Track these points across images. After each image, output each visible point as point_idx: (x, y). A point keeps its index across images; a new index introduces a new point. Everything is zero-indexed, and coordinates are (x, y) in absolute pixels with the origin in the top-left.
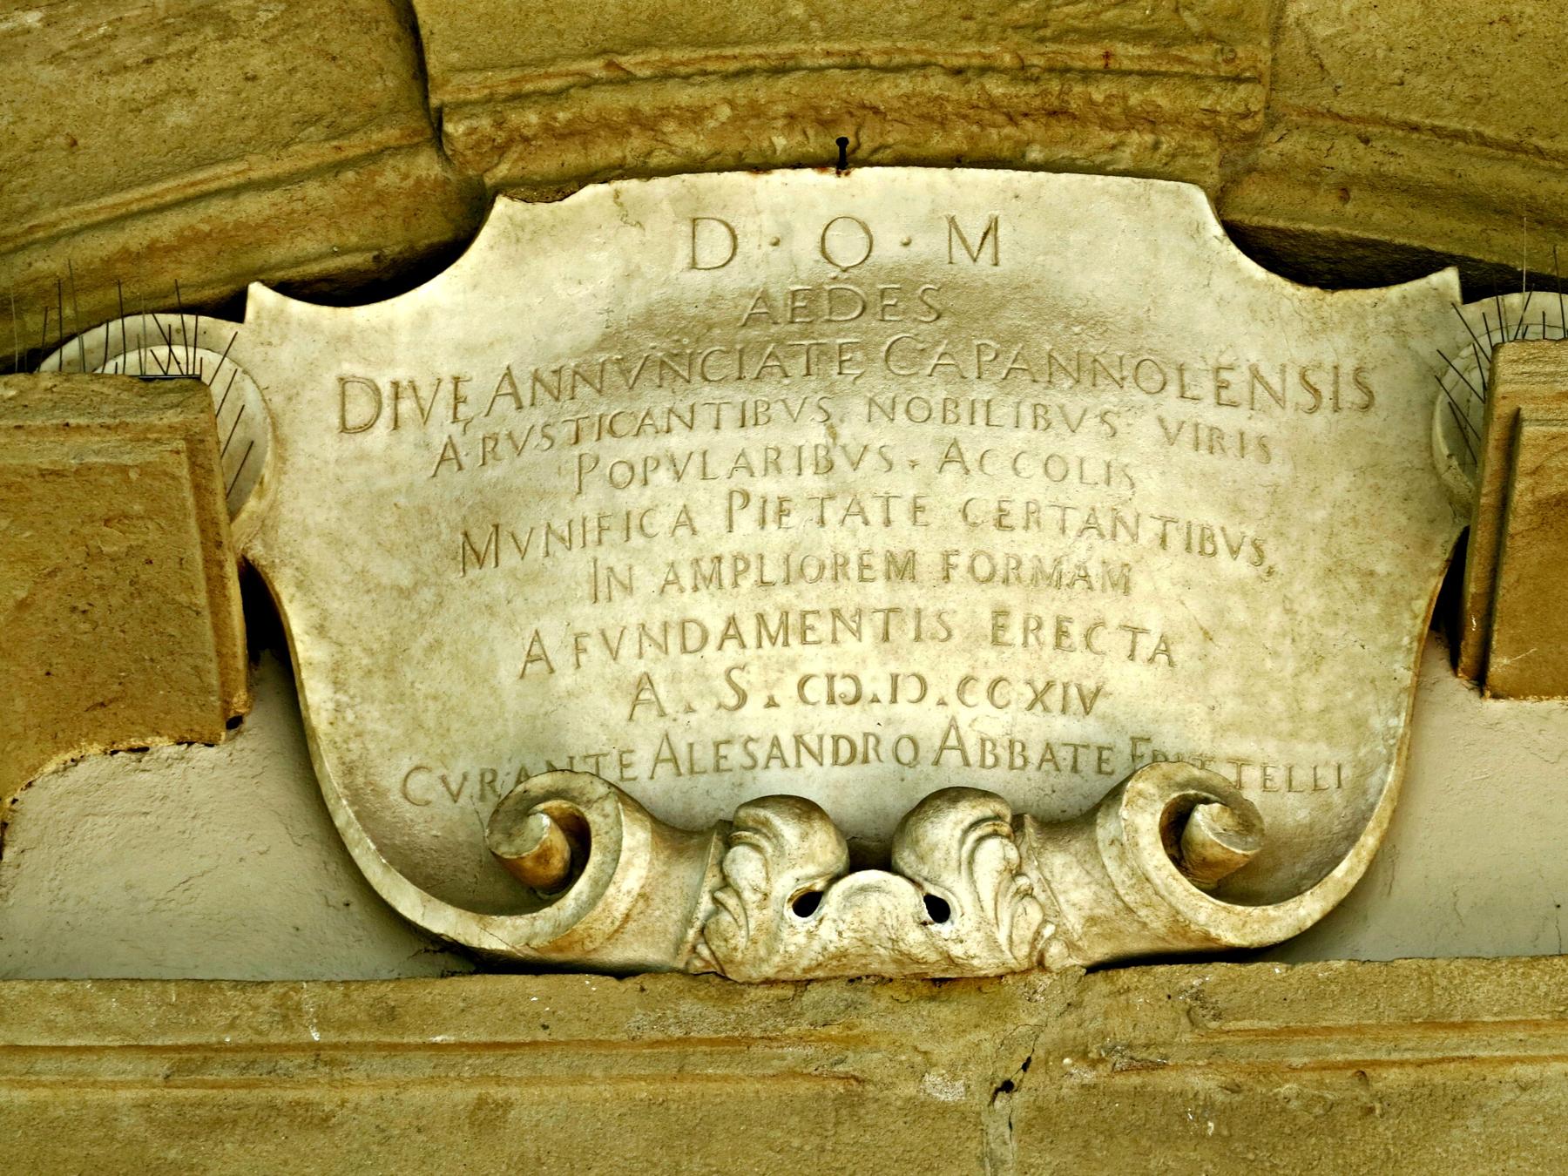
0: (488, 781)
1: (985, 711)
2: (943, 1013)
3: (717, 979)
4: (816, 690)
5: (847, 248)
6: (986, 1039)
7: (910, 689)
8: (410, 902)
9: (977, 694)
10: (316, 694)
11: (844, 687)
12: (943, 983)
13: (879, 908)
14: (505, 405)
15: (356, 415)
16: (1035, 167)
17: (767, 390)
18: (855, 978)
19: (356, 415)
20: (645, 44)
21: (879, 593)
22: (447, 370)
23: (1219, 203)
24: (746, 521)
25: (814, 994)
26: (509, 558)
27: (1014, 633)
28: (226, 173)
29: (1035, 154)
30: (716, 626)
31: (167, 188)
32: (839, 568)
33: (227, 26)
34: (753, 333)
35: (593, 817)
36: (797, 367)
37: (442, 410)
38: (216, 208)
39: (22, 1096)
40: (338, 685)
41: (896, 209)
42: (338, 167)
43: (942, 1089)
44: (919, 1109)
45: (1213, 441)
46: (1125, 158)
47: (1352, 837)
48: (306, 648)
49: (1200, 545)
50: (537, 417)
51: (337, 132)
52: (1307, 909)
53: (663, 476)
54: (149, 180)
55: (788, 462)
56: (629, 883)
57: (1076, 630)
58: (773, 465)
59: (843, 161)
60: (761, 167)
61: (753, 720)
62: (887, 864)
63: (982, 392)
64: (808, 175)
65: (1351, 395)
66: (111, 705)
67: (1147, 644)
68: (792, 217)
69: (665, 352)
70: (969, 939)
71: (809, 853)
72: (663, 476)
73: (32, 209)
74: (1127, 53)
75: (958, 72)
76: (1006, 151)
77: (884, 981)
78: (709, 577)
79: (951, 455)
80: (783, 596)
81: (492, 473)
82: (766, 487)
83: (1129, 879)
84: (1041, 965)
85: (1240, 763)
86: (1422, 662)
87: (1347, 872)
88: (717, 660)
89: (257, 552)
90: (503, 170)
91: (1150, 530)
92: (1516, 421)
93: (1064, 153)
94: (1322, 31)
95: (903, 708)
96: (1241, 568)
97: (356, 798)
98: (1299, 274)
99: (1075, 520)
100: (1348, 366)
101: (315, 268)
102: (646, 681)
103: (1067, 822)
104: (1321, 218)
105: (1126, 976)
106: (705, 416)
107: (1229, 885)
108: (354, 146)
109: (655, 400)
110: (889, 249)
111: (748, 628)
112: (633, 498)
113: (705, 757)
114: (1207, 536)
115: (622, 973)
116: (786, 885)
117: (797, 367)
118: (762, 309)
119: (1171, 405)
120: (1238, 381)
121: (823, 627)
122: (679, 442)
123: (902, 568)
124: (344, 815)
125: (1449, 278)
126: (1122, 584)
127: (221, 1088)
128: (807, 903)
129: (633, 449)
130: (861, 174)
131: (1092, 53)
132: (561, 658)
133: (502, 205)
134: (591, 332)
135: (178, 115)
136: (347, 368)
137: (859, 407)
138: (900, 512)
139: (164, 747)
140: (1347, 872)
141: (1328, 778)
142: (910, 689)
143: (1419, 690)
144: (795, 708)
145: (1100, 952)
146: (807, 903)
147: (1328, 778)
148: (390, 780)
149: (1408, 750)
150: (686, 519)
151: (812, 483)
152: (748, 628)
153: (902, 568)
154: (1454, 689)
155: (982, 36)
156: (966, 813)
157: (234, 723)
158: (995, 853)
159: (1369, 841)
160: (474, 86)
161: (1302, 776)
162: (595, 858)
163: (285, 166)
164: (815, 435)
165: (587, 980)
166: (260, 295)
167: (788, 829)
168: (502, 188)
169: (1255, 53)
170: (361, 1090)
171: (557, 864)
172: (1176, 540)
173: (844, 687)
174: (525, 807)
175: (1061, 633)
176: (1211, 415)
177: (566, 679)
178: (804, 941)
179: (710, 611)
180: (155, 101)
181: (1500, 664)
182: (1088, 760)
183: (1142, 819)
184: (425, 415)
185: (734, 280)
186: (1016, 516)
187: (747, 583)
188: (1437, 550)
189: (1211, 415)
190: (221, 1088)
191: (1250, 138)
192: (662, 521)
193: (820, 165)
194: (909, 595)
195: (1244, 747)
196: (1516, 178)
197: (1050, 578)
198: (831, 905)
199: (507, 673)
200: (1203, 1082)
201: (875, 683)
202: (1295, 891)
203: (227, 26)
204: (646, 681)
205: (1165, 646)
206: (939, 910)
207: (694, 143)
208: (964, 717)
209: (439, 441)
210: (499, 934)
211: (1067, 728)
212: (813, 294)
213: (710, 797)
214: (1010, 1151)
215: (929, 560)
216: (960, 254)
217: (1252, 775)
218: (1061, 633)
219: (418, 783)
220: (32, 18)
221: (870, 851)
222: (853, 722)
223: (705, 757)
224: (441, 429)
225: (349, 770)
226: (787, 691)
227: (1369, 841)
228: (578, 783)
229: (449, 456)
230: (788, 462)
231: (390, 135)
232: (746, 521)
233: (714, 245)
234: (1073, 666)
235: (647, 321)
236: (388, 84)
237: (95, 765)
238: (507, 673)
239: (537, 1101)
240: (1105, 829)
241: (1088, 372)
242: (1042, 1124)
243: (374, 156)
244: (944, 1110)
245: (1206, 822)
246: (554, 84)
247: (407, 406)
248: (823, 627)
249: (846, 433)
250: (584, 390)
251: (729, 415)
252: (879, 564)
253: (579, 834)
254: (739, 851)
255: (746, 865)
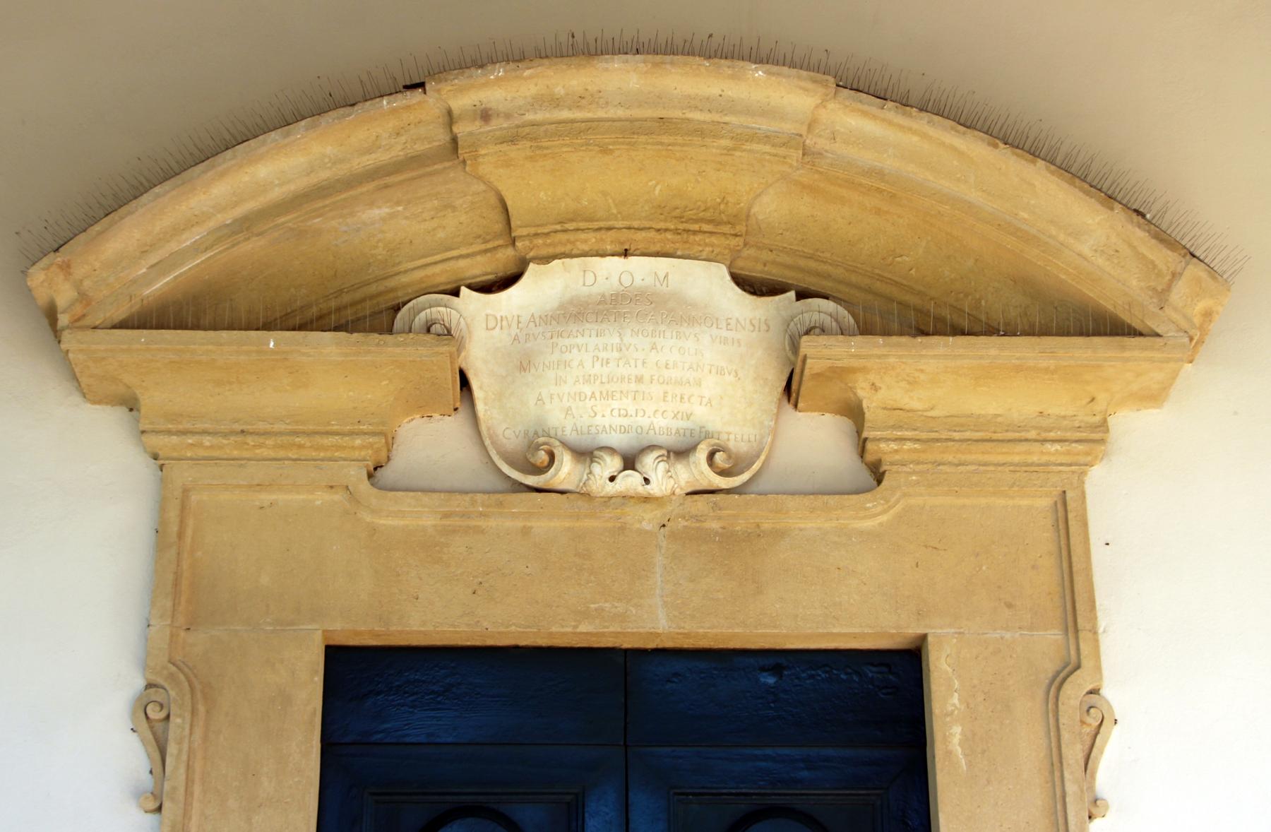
0: (526, 433)
1: (661, 422)
2: (648, 506)
3: (587, 496)
4: (616, 413)
5: (627, 282)
6: (658, 513)
7: (641, 413)
8: (506, 469)
9: (659, 415)
10: (480, 407)
11: (623, 412)
12: (647, 499)
13: (630, 482)
14: (532, 325)
15: (491, 325)
16: (679, 257)
17: (604, 326)
18: (625, 498)
19: (491, 325)
20: (572, 220)
21: (633, 386)
22: (515, 314)
23: (729, 268)
24: (598, 365)
25: (613, 500)
26: (533, 371)
27: (669, 398)
28: (455, 253)
29: (679, 253)
30: (589, 394)
31: (438, 258)
32: (623, 379)
33: (454, 209)
34: (600, 307)
35: (555, 451)
36: (612, 318)
37: (514, 325)
38: (451, 264)
39: (402, 523)
40: (486, 404)
41: (641, 270)
42: (486, 251)
43: (646, 526)
44: (641, 532)
45: (725, 341)
46: (704, 255)
47: (758, 456)
48: (478, 393)
49: (720, 372)
50: (540, 329)
51: (486, 242)
52: (745, 477)
53: (575, 351)
54: (433, 255)
55: (609, 348)
56: (565, 472)
57: (686, 398)
58: (605, 349)
59: (626, 254)
60: (603, 255)
61: (599, 420)
62: (634, 469)
63: (663, 328)
64: (616, 258)
65: (764, 327)
66: (422, 405)
67: (705, 401)
68: (611, 273)
69: (577, 312)
70: (655, 489)
71: (613, 464)
72: (575, 351)
73: (399, 263)
74: (706, 227)
75: (659, 230)
76: (671, 251)
77: (632, 497)
78: (588, 380)
79: (654, 348)
80: (607, 386)
81: (528, 345)
82: (603, 355)
83: (697, 472)
84: (674, 494)
85: (729, 433)
86: (779, 407)
87: (756, 467)
88: (589, 403)
89: (464, 366)
90: (531, 254)
91: (707, 368)
92: (805, 358)
93: (687, 252)
94: (760, 217)
95: (639, 418)
96: (732, 378)
97: (491, 437)
98: (754, 293)
99: (687, 366)
100: (763, 319)
101: (479, 279)
102: (569, 408)
103: (680, 453)
104: (756, 271)
105: (696, 497)
106: (587, 332)
107: (723, 473)
108: (489, 245)
109: (573, 327)
110: (638, 282)
111: (598, 395)
112: (567, 356)
113: (585, 430)
114: (722, 369)
115: (562, 492)
116: (607, 474)
117: (612, 318)
118: (603, 300)
119: (714, 331)
120: (733, 322)
121: (618, 395)
122: (580, 340)
123: (639, 380)
124: (487, 442)
125: (792, 294)
126: (699, 384)
127: (455, 522)
128: (612, 479)
129: (567, 342)
130: (630, 258)
131: (696, 227)
132: (547, 400)
133: (532, 266)
134: (556, 305)
135: (441, 234)
136: (489, 312)
137: (629, 331)
138: (639, 363)
139: (437, 416)
140: (756, 467)
141: (752, 438)
142: (641, 413)
143: (777, 417)
144: (612, 420)
145: (689, 490)
146: (612, 479)
147: (752, 438)
148: (500, 432)
149: (775, 433)
150: (581, 364)
151: (616, 354)
152: (598, 395)
153: (639, 380)
154: (788, 408)
155: (665, 221)
156: (655, 454)
157: (456, 409)
158: (662, 466)
159: (763, 457)
160: (524, 232)
161: (746, 437)
162: (556, 463)
163: (470, 251)
164: (616, 340)
165: (553, 495)
166: (464, 290)
167: (608, 458)
168: (533, 259)
169: (740, 228)
170: (493, 523)
171: (546, 463)
172: (714, 371)
173: (623, 412)
174: (537, 447)
175: (682, 398)
176: (725, 333)
177: (548, 406)
178: (611, 488)
179: (587, 390)
180: (434, 229)
181: (800, 405)
182: (688, 433)
183: (701, 455)
184: (510, 326)
185: (596, 290)
186: (671, 365)
187: (598, 382)
188: (804, 206)
189: (725, 333)
190: (455, 522)
191: (739, 251)
192: (575, 364)
193: (619, 255)
194: (642, 387)
195: (730, 429)
196: (812, 264)
197: (679, 383)
198: (618, 480)
199: (532, 402)
200: (715, 525)
201: (631, 411)
202: (741, 472)
203: (454, 209)
204: (569, 408)
205: (710, 401)
206: (647, 481)
207: (586, 248)
208: (655, 421)
209: (513, 334)
210: (531, 480)
211: (683, 424)
212: (617, 295)
213: (585, 442)
214: (664, 544)
215: (647, 378)
216: (658, 284)
217: (732, 437)
218: (682, 398)
219: (507, 432)
220: (400, 208)
221: (630, 463)
222: (625, 422)
223: (585, 430)
224: (514, 331)
225: (489, 429)
226: (608, 413)
227: (763, 457)
228: (552, 440)
229: (516, 338)
230: (609, 348)
231: (500, 242)
232: (598, 365)
233: (590, 279)
234: (685, 407)
235: (571, 302)
236: (499, 227)
237: (418, 421)
238: (532, 402)
239: (540, 526)
240: (692, 459)
241: (692, 321)
242: (673, 536)
243: (495, 248)
244: (647, 532)
245: (719, 457)
246: (546, 231)
247: (505, 323)
248: (618, 395)
249: (625, 339)
250: (554, 322)
251: (594, 333)
252: (633, 378)
253: (552, 456)
254: (595, 464)
255: (596, 468)
